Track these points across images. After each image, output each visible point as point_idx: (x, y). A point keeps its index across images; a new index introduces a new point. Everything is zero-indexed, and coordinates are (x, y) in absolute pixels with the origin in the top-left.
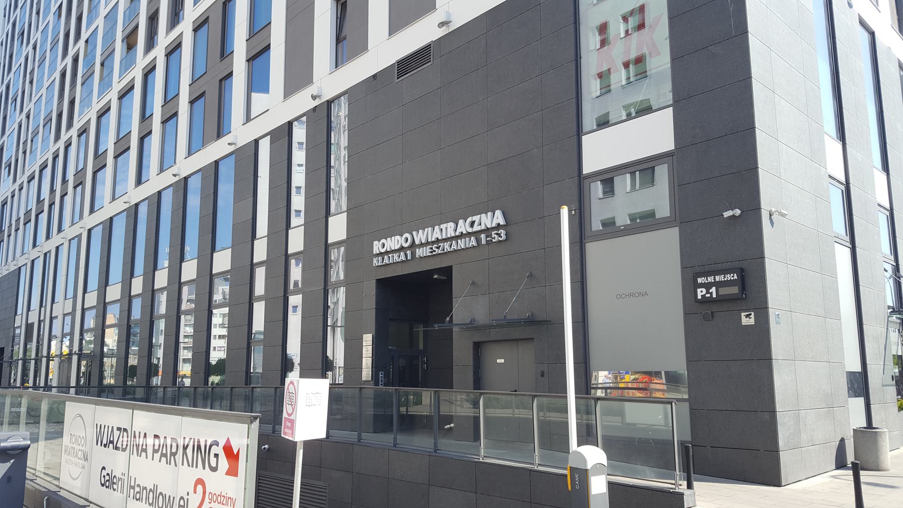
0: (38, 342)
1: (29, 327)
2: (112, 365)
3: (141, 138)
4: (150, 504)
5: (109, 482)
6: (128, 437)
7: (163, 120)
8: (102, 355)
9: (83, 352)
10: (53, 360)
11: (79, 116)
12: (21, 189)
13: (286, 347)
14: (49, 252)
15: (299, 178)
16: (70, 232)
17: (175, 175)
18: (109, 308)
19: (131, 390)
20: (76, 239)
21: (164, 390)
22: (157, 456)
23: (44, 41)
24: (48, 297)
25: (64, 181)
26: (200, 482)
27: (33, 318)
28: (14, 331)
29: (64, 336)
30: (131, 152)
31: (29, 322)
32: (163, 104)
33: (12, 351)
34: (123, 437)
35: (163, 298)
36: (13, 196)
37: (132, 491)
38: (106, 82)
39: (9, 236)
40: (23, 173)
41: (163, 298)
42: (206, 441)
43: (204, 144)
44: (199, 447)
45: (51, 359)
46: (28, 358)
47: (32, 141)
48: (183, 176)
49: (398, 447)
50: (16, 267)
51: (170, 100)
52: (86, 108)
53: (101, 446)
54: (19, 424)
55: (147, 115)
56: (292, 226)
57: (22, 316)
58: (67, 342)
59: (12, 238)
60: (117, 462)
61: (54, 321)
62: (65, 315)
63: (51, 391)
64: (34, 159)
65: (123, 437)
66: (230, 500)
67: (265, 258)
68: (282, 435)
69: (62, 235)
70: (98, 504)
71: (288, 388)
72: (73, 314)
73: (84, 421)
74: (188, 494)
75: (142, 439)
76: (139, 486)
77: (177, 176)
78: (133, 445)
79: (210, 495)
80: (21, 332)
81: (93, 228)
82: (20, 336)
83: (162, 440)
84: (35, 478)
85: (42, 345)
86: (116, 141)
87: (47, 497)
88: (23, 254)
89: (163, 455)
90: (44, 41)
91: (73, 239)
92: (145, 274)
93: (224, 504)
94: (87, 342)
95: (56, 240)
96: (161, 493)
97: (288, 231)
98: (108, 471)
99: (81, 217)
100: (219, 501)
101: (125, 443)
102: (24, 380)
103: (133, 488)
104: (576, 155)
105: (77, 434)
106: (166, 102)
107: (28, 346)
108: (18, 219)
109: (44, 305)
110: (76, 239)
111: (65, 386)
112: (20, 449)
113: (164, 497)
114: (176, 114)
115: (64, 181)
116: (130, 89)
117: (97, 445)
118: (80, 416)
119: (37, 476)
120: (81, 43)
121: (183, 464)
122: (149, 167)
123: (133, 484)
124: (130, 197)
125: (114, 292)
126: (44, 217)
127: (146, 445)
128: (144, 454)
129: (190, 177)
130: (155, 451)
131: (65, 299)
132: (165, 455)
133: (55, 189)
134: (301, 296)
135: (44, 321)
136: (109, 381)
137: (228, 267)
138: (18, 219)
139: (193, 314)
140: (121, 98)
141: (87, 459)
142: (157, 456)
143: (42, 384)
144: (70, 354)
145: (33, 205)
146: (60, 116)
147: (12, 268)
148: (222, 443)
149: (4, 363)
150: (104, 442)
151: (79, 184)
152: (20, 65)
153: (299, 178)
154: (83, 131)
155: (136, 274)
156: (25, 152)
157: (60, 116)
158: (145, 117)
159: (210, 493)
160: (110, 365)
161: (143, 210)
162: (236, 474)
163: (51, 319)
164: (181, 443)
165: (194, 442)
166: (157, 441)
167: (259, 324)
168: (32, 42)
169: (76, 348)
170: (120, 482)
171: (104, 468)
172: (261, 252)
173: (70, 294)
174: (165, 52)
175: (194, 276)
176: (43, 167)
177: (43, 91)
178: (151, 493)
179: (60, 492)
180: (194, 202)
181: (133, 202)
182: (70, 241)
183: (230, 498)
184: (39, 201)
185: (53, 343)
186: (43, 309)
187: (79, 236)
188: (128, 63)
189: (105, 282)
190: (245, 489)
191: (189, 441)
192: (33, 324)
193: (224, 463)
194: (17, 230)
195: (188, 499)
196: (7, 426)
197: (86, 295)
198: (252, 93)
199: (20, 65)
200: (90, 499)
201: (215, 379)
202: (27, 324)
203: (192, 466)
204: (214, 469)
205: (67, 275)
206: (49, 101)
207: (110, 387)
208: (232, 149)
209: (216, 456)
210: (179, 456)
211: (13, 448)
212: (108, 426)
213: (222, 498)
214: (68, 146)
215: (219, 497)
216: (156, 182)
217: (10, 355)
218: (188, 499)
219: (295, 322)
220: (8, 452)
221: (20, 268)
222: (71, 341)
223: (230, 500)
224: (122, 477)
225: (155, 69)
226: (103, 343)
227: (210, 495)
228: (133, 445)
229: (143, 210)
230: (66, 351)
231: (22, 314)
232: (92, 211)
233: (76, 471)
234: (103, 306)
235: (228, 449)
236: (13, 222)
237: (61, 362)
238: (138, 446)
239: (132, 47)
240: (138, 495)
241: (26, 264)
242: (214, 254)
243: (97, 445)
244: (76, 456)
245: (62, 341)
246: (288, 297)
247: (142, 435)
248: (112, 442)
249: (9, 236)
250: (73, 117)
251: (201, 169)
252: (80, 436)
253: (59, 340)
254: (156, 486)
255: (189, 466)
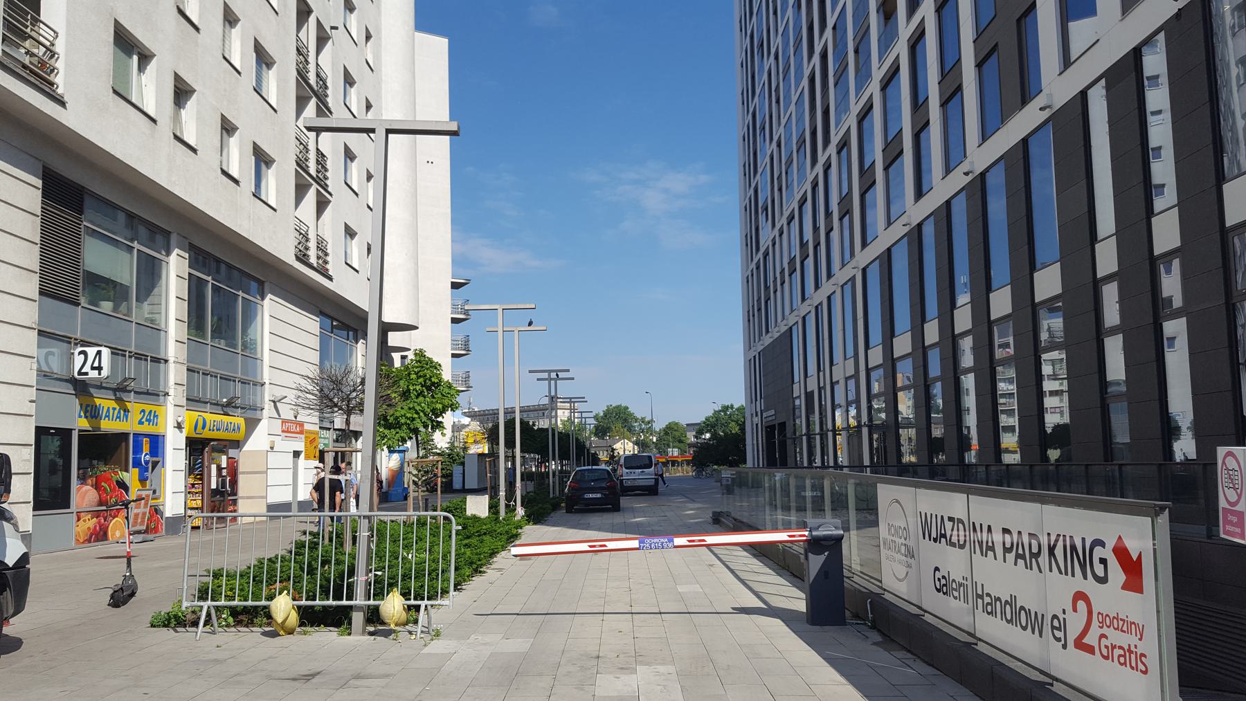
0: (821, 413)
1: (809, 396)
2: (910, 438)
3: (916, 135)
4: (1008, 621)
5: (944, 587)
6: (965, 530)
7: (942, 102)
8: (897, 426)
9: (874, 423)
10: (840, 435)
11: (836, 127)
12: (781, 234)
13: (1167, 402)
14: (821, 304)
15: (1160, 132)
16: (841, 276)
17: (966, 174)
18: (899, 365)
19: (938, 469)
20: (850, 283)
21: (986, 469)
22: (1011, 557)
23: (786, 44)
24: (826, 359)
25: (828, 214)
26: (1080, 596)
27: (812, 386)
28: (794, 402)
29: (848, 404)
30: (877, 187)
31: (808, 391)
32: (940, 79)
33: (794, 425)
34: (958, 530)
35: (967, 344)
36: (774, 245)
37: (980, 601)
38: (863, 75)
39: (775, 292)
40: (782, 214)
41: (967, 344)
42: (1083, 539)
43: (1004, 118)
44: (1073, 548)
45: (837, 433)
46: (811, 433)
47: (787, 173)
48: (978, 172)
49: (1214, 539)
50: (786, 328)
51: (950, 72)
52: (843, 115)
53: (930, 540)
54: (805, 510)
55: (921, 101)
56: (1156, 211)
57: (800, 384)
58: (853, 412)
59: (779, 293)
60: (954, 563)
61: (836, 387)
62: (847, 379)
63: (842, 470)
64: (791, 195)
65: (958, 530)
66: (1133, 626)
67: (1116, 269)
68: (1222, 536)
69: (832, 280)
70: (946, 619)
71: (1224, 463)
72: (856, 376)
73: (902, 507)
74: (1064, 612)
75: (985, 535)
76: (988, 595)
77: (971, 174)
78: (974, 542)
79: (1100, 616)
80: (801, 403)
81: (867, 266)
82: (801, 408)
83: (1015, 536)
84: (851, 575)
85: (826, 416)
86: (884, 147)
87: (870, 600)
88: (792, 311)
89: (1018, 556)
90: (786, 44)
91: (846, 283)
92: (940, 317)
93: (1124, 632)
94: (875, 410)
95: (827, 288)
96: (1022, 608)
97: (989, 296)
98: (943, 572)
99: (852, 255)
100: (1116, 627)
101: (962, 539)
102: (811, 461)
103: (981, 597)
104: (1090, 265)
105: (897, 524)
106: (944, 75)
107: (811, 419)
108: (783, 271)
109: (822, 369)
110: (850, 283)
111: (858, 465)
112: (833, 540)
113: (1028, 613)
114: (959, 88)
115: (828, 214)
116: (895, 71)
117: (924, 538)
118: (897, 501)
119: (853, 573)
120: (829, 32)
121: (1051, 570)
122: (930, 171)
123: (980, 592)
124: (909, 217)
125: (903, 345)
126: (810, 262)
127: (993, 543)
128: (990, 553)
129: (988, 171)
130: (1007, 550)
131: (845, 359)
132: (1023, 557)
133: (818, 226)
134: (1184, 319)
135: (824, 387)
136: (909, 458)
137: (1058, 290)
138: (783, 271)
139: (1013, 363)
140: (884, 88)
141: (913, 556)
142: (1011, 557)
143: (832, 464)
144: (859, 426)
145: (796, 251)
146: (814, 133)
147: (784, 329)
148: (1111, 543)
149: (787, 440)
150: (934, 535)
151: (846, 212)
152: (764, 84)
153: (1160, 132)
154: (844, 144)
155: (928, 317)
156: (780, 190)
157: (814, 133)
158: (919, 105)
159: (1099, 613)
160: (907, 438)
161: (929, 231)
162: (1139, 589)
163: (833, 385)
164: (1044, 541)
165: (1064, 541)
166: (1007, 536)
167: (1116, 367)
168: (773, 51)
169: (865, 419)
170: (962, 588)
171: (937, 569)
172: (1107, 259)
173: (850, 352)
174: (935, 7)
175: (1175, 242)
176: (803, 202)
177: (792, 107)
178: (1008, 606)
179: (884, 594)
180: (998, 207)
181: (915, 223)
182: (842, 286)
183: (1134, 623)
184: (803, 245)
185: (837, 414)
186: (821, 374)
187: (853, 279)
188: (887, 39)
189: (890, 333)
190: (1158, 612)
191: (1057, 541)
192: (812, 392)
193: (1117, 575)
194: (783, 283)
195: (1064, 619)
196: (811, 512)
197: (807, 379)
198: (1069, 24)
199: (764, 84)
200: (924, 607)
201: (1054, 454)
202: (806, 393)
203: (1066, 574)
204: (1103, 580)
205: (844, 330)
206: (800, 119)
207: (911, 465)
208: (1046, 114)
209: (1103, 561)
210: (1044, 558)
211: (826, 538)
212: (936, 515)
213: (1121, 623)
214: (827, 167)
215: (1115, 620)
216: (943, 188)
217: (792, 430)
218: (1064, 619)
219: (1178, 363)
220: (822, 542)
221: (791, 328)
222: (858, 409)
223: (1133, 626)
224: (963, 582)
225: (899, 69)
226: (896, 411)
227: (1100, 616)
228: (974, 542)
229: (929, 231)
230: (853, 422)
231: (800, 382)
232: (864, 244)
233: (901, 571)
234: (891, 363)
235: (1121, 552)
236: (778, 275)
237: (849, 437)
238: (981, 543)
239: (891, 15)
240: (989, 608)
241: (797, 322)
242: (1035, 274)
243: (924, 538)
244: (899, 551)
245: (847, 411)
246: (1103, 340)
247: (985, 529)
248: (944, 536)
249: (775, 292)
250: (830, 130)
251: (964, 187)
252: (900, 527)
253: (844, 409)
254: (1014, 598)
255: (1061, 573)
